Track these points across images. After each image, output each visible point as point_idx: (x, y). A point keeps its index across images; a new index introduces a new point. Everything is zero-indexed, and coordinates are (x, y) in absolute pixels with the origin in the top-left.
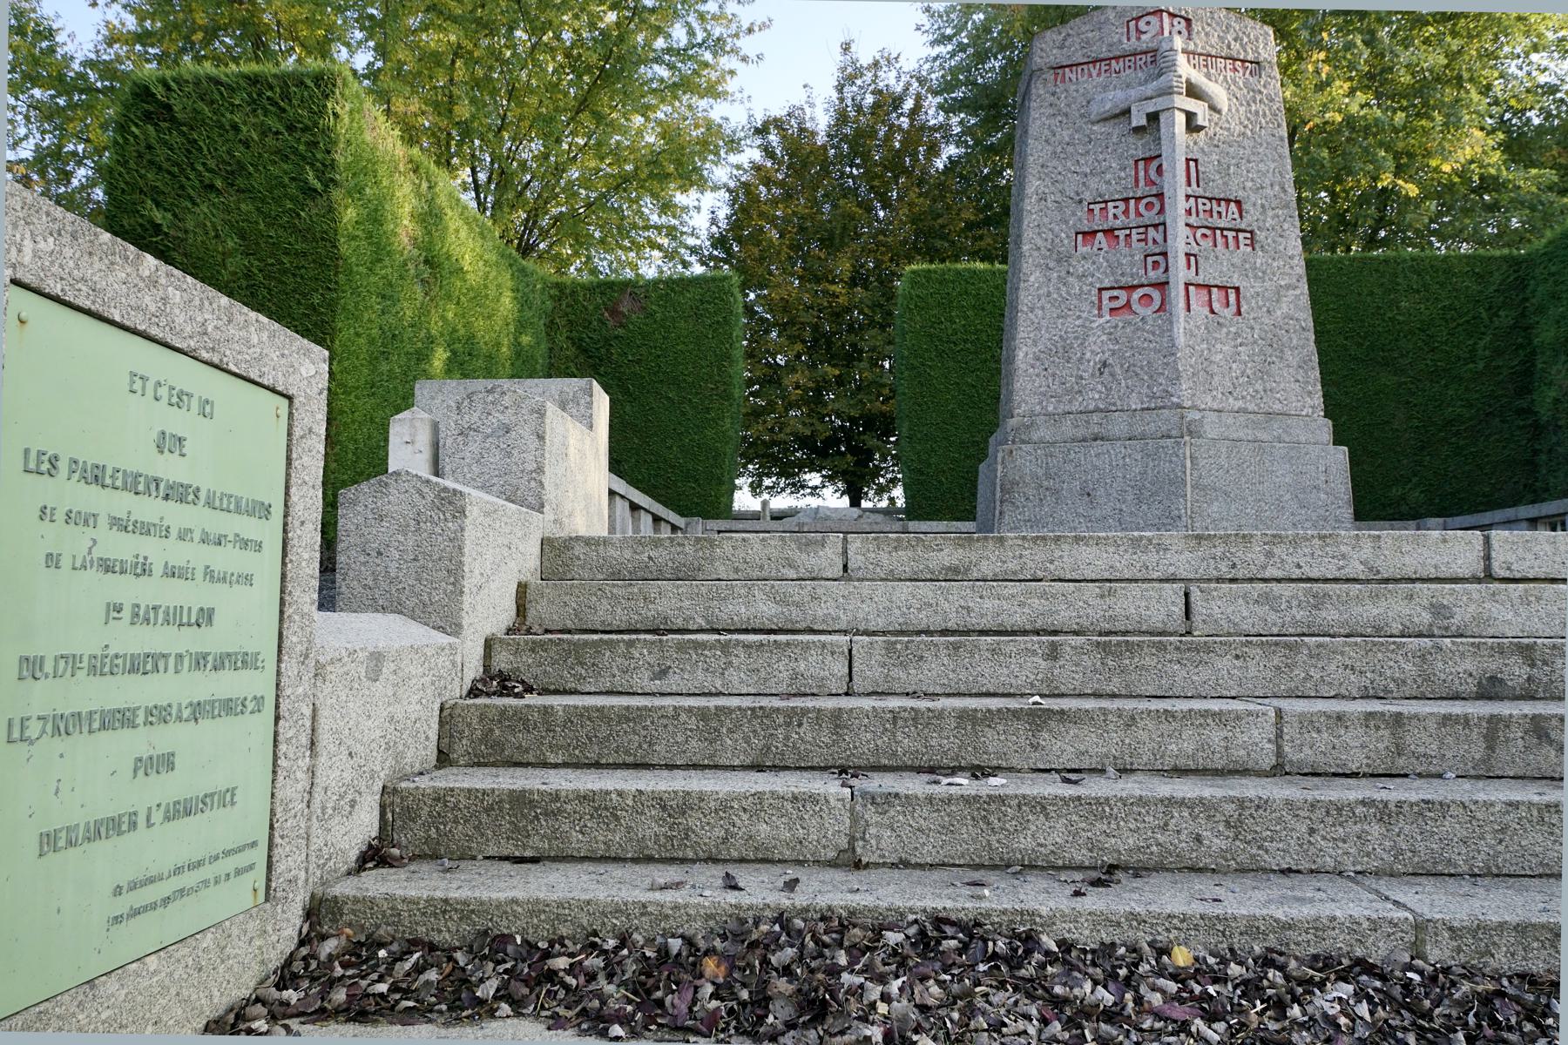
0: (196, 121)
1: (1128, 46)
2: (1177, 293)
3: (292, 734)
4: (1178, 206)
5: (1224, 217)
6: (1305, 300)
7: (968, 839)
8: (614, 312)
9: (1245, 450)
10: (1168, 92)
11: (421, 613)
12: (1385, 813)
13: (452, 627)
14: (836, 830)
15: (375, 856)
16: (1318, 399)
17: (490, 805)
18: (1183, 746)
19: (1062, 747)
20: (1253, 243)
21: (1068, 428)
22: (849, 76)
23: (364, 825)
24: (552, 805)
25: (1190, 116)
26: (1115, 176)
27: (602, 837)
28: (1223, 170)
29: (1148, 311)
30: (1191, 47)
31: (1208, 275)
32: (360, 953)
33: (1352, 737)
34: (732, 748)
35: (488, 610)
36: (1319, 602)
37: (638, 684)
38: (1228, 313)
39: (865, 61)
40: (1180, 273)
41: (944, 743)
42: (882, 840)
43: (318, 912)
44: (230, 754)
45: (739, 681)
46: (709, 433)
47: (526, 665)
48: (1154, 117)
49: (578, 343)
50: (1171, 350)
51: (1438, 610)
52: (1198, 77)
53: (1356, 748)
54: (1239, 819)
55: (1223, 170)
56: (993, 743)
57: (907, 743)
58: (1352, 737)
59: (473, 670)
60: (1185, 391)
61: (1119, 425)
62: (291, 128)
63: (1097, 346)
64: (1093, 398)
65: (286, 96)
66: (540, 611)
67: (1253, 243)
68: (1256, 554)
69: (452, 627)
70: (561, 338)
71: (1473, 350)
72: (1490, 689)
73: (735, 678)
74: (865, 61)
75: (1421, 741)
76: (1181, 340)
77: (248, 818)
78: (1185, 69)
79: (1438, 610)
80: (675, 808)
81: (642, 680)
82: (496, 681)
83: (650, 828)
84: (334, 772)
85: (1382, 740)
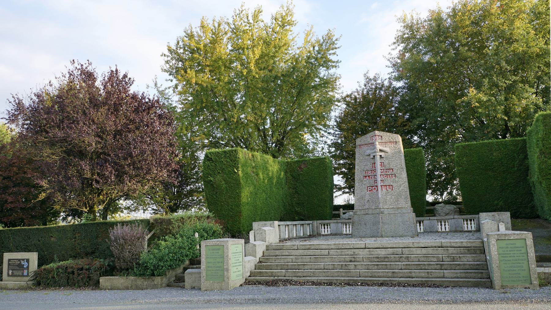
0: (216, 161)
1: (371, 142)
2: (379, 188)
3: (244, 267)
4: (379, 172)
5: (388, 172)
6: (408, 186)
7: (293, 275)
8: (300, 168)
9: (392, 215)
10: (375, 152)
11: (253, 256)
12: (324, 272)
13: (256, 257)
14: (284, 274)
15: (250, 276)
16: (409, 204)
17: (258, 272)
18: (316, 267)
19: (306, 267)
20: (395, 176)
21: (362, 212)
22: (369, 80)
23: (249, 274)
24: (262, 272)
25: (381, 156)
26: (369, 167)
27: (267, 275)
28: (389, 164)
29: (375, 191)
30: (384, 141)
31: (386, 183)
32: (249, 282)
33: (330, 266)
34: (279, 268)
35: (259, 254)
36: (342, 252)
37: (273, 262)
38: (390, 190)
39: (372, 77)
40: (379, 184)
41: (296, 267)
42: (287, 275)
43: (246, 279)
44: (240, 268)
45: (282, 262)
46: (324, 196)
47: (263, 260)
48: (374, 156)
49: (292, 175)
50: (378, 198)
51: (354, 253)
52: (381, 148)
53: (331, 267)
54: (314, 273)
55: (389, 164)
56: (300, 267)
57: (293, 267)
58: (330, 266)
59: (258, 261)
60: (381, 206)
61: (370, 212)
62: (231, 161)
63: (367, 198)
64: (367, 207)
65: (230, 155)
66: (265, 254)
67: (395, 176)
68: (341, 246)
69: (256, 257)
70: (288, 175)
71: (514, 165)
72: (351, 261)
73: (282, 261)
74: (372, 77)
75: (336, 266)
76: (380, 196)
77: (241, 272)
78: (379, 147)
79: (354, 253)
80: (272, 273)
81: (273, 261)
82: (260, 262)
83: (270, 274)
84: (247, 270)
85: (333, 266)
